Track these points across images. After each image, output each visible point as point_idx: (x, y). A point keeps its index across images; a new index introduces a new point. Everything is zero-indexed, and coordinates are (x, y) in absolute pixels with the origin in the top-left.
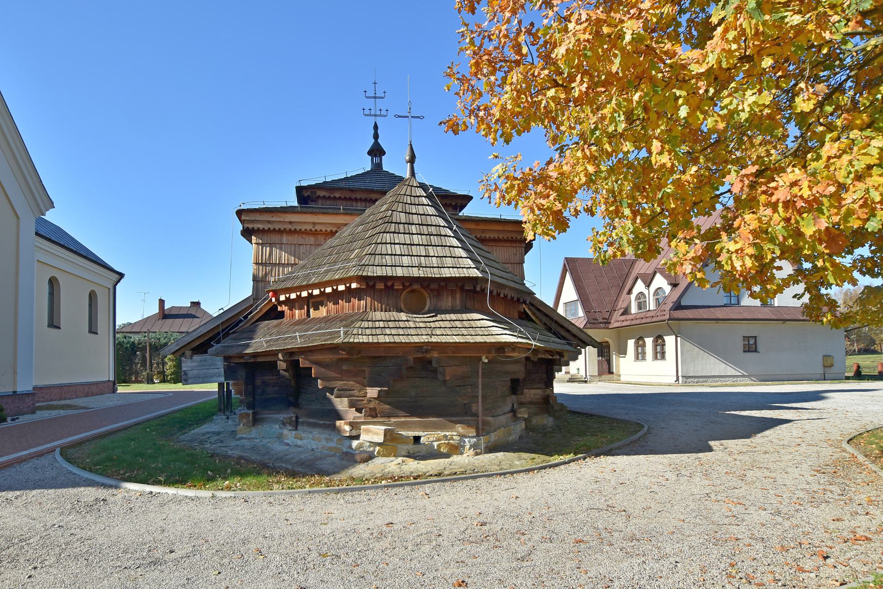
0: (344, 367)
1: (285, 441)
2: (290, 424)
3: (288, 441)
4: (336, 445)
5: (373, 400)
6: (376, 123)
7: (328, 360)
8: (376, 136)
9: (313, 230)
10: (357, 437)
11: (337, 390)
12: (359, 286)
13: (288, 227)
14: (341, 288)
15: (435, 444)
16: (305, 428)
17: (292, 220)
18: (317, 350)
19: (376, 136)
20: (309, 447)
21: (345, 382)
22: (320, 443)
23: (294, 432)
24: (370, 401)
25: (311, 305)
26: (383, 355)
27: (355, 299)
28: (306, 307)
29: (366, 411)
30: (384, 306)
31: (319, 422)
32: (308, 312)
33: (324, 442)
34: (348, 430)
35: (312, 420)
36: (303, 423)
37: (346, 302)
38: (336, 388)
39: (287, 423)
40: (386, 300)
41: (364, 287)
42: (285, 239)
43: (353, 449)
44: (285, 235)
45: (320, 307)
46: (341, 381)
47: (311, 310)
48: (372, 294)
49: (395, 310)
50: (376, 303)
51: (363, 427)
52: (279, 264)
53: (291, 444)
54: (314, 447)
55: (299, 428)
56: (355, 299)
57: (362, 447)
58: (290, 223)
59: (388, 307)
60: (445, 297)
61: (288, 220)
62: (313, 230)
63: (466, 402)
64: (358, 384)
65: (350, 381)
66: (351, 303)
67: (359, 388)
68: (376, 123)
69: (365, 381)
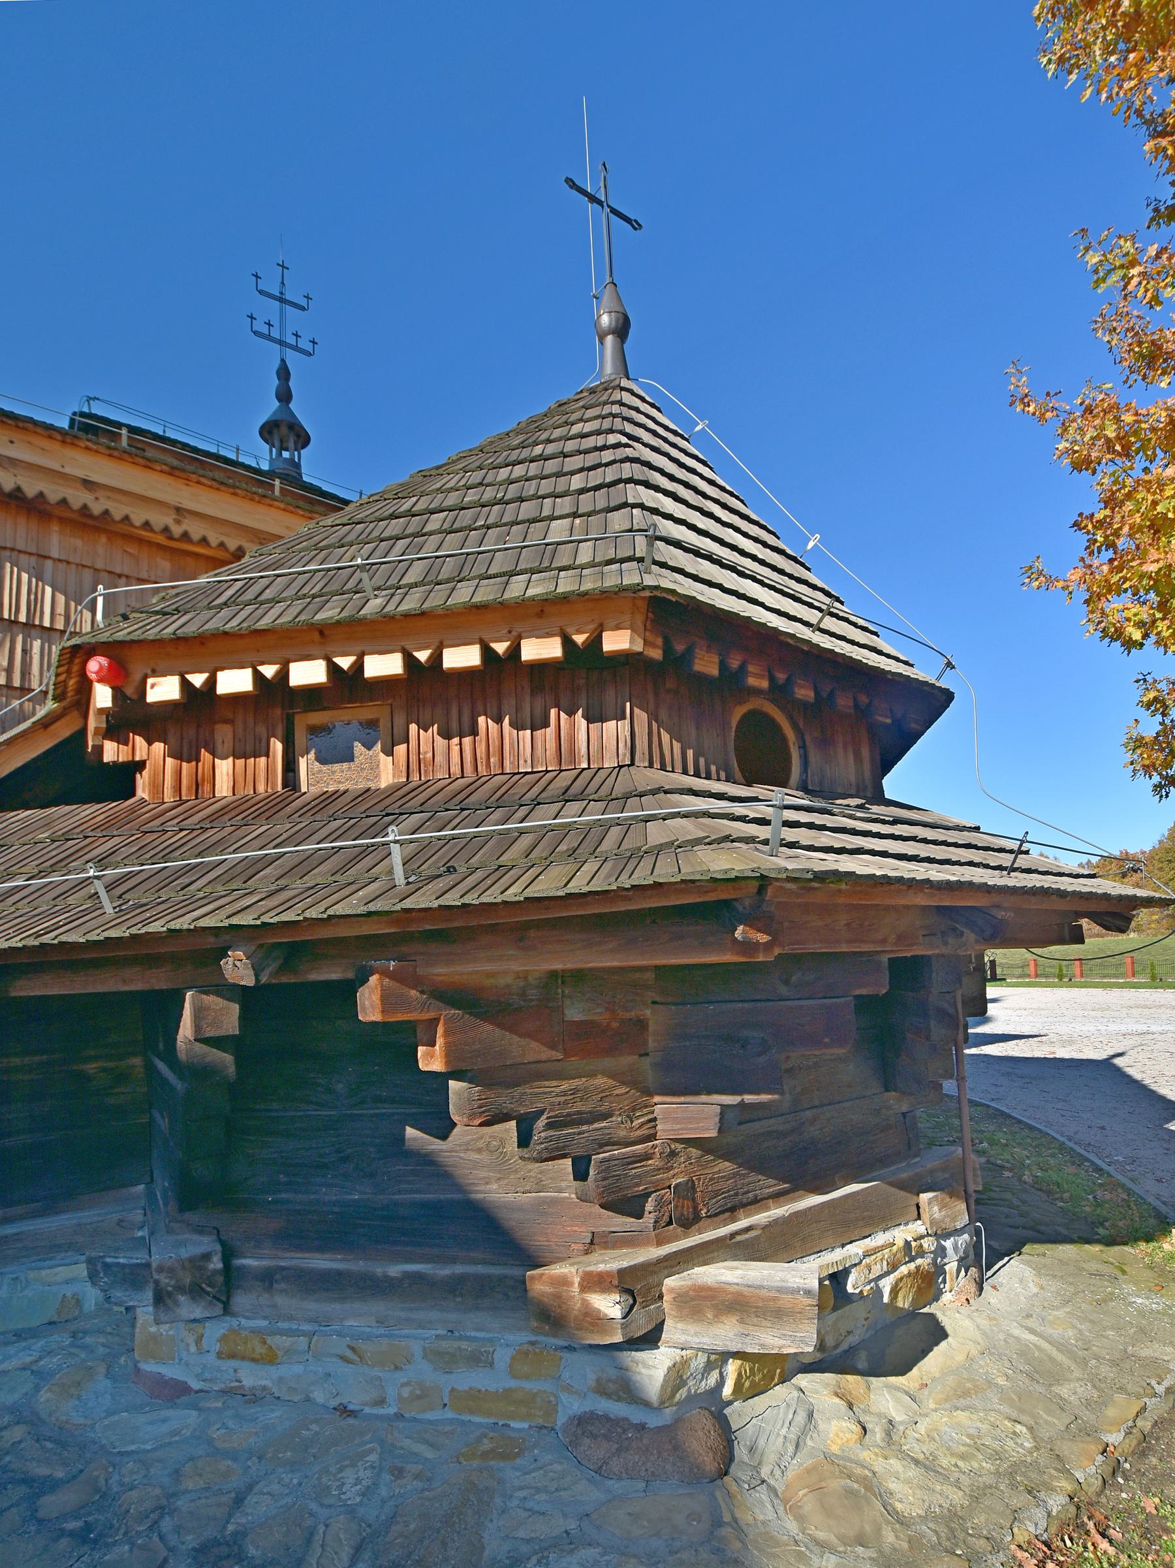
0: (575, 1013)
1: (149, 1367)
2: (195, 1292)
3: (171, 1372)
4: (513, 1383)
5: (680, 1147)
6: (283, 361)
7: (509, 980)
8: (285, 396)
9: (177, 531)
10: (651, 1339)
11: (550, 1126)
12: (639, 647)
13: (78, 498)
14: (536, 649)
15: (886, 1285)
16: (280, 1300)
17: (94, 477)
18: (493, 929)
19: (285, 396)
20: (319, 1396)
21: (576, 1083)
22: (401, 1377)
23: (215, 1331)
24: (673, 1154)
25: (300, 737)
26: (844, 948)
27: (571, 713)
28: (277, 747)
29: (660, 1204)
30: (690, 753)
31: (379, 1270)
32: (290, 767)
33: (423, 1371)
34: (616, 1312)
35: (321, 1262)
36: (268, 1279)
37: (517, 726)
38: (540, 1113)
39: (180, 1289)
40: (693, 732)
41: (656, 654)
42: (56, 542)
43: (647, 1404)
44: (55, 527)
45: (358, 748)
46: (560, 1076)
47: (303, 763)
48: (652, 706)
49: (723, 775)
50: (665, 737)
51: (671, 1283)
52: (29, 626)
53: (195, 1385)
54: (355, 1398)
55: (241, 1300)
56: (571, 713)
57: (683, 1383)
58: (88, 484)
59: (702, 761)
60: (841, 751)
61: (81, 473)
62: (177, 531)
63: (904, 1109)
64: (623, 1083)
65: (592, 1075)
66: (550, 731)
67: (626, 1104)
68: (283, 361)
69: (651, 1078)
